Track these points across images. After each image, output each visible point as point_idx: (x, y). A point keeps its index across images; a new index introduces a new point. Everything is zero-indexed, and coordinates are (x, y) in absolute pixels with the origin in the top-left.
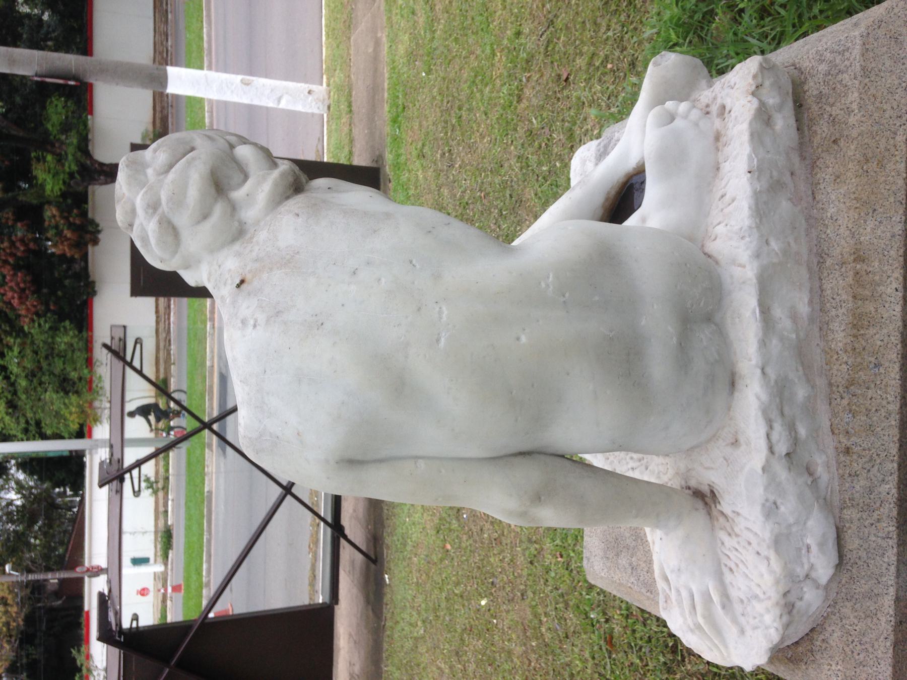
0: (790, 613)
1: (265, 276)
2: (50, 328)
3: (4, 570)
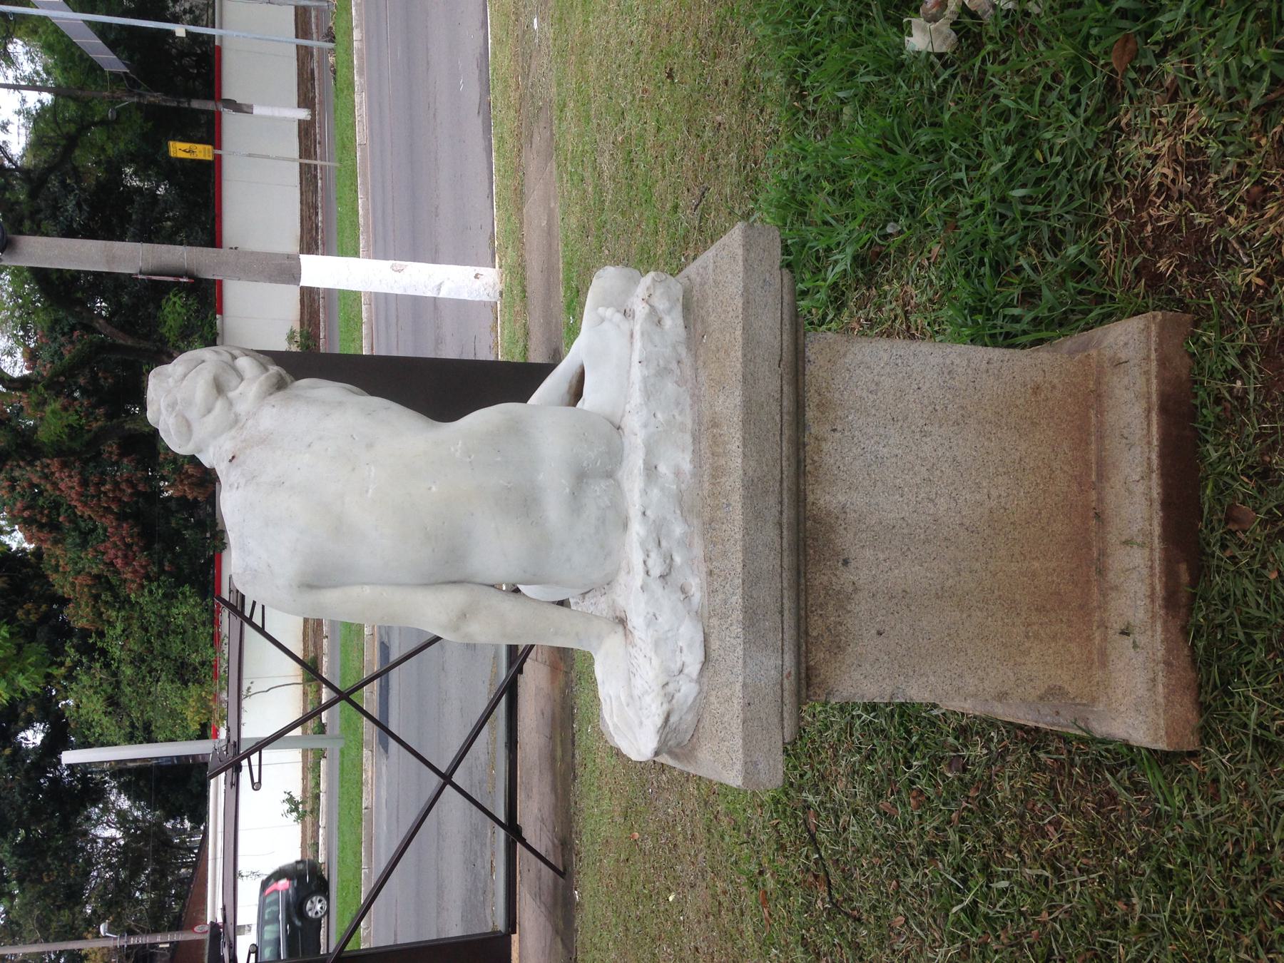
0: (670, 702)
1: (248, 452)
2: (165, 595)
3: (99, 932)
